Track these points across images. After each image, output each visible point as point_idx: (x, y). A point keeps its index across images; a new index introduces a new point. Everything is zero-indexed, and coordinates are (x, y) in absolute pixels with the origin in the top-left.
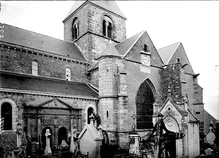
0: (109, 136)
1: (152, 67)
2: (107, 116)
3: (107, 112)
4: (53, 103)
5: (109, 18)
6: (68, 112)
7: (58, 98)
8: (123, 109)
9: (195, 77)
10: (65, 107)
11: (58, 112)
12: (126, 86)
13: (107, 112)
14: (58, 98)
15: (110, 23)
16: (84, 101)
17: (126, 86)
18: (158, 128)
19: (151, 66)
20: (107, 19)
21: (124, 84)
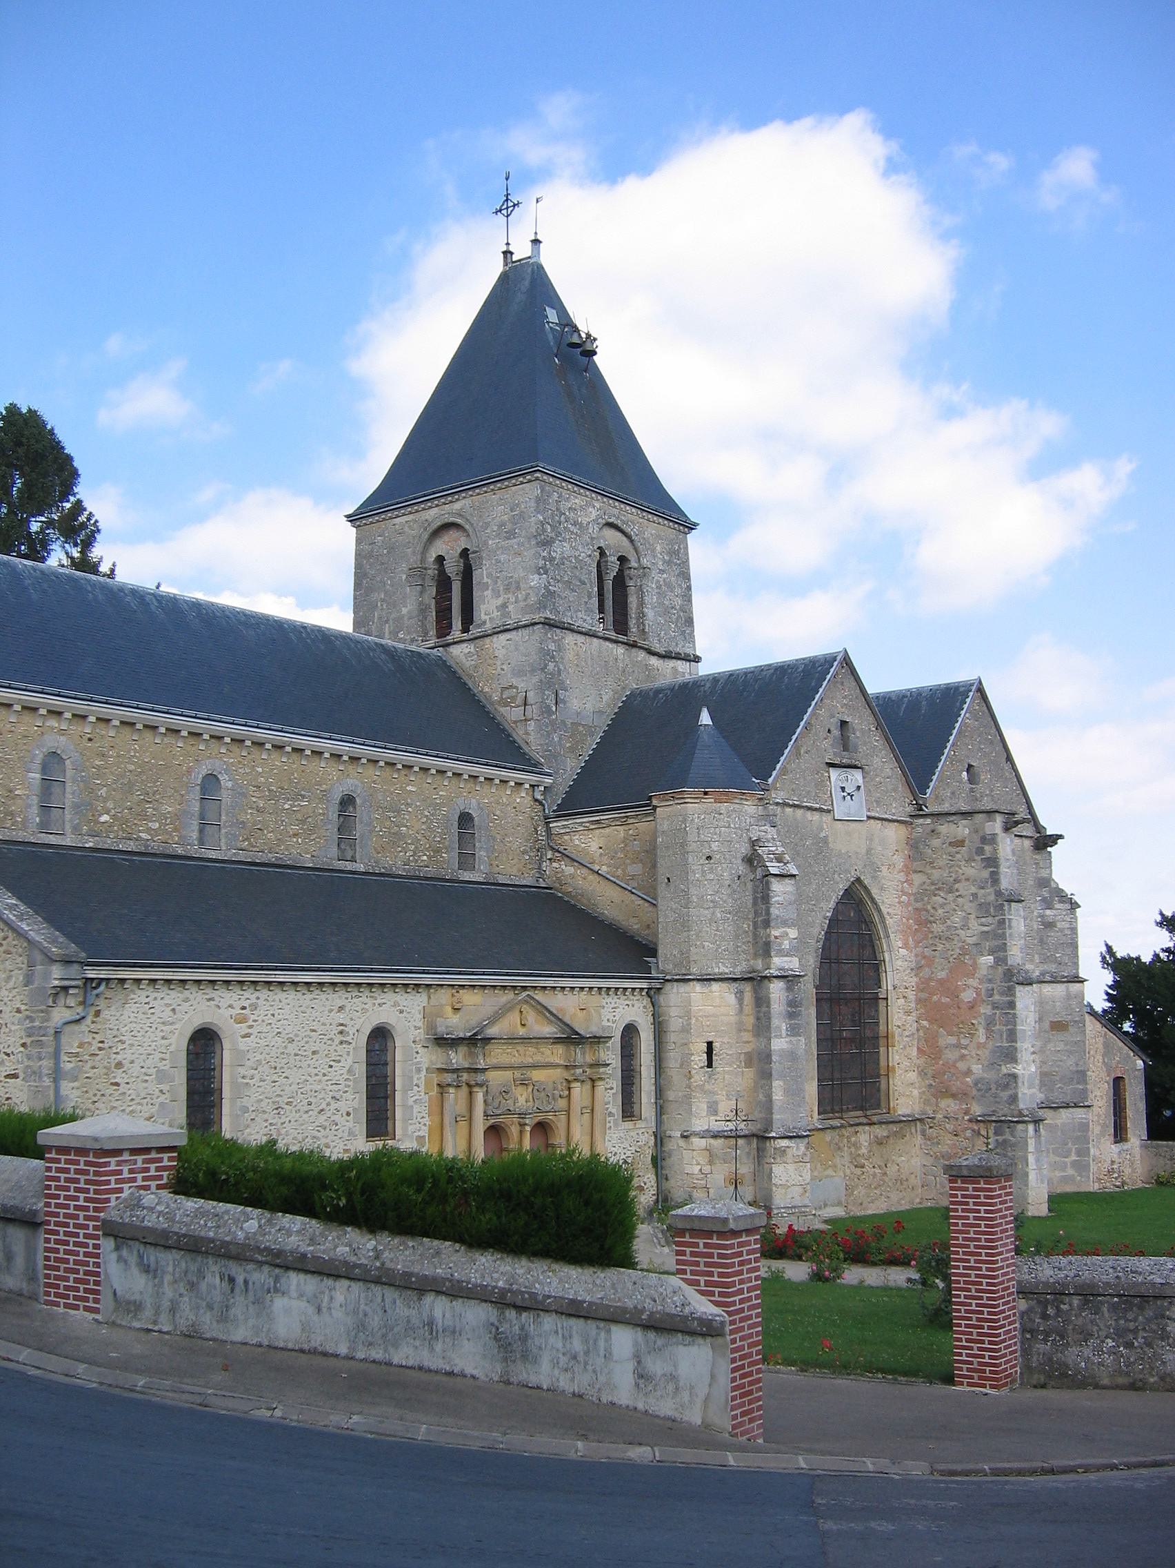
0: (836, 1182)
1: (872, 821)
2: (710, 1065)
3: (710, 1044)
4: (514, 1017)
5: (619, 534)
6: (557, 1054)
7: (539, 996)
8: (784, 1035)
9: (1044, 842)
10: (548, 1030)
11: (529, 1055)
12: (793, 933)
13: (710, 1044)
14: (539, 996)
15: (622, 559)
16: (609, 1000)
17: (793, 933)
18: (105, 800)
19: (869, 818)
20: (612, 537)
21: (785, 923)
